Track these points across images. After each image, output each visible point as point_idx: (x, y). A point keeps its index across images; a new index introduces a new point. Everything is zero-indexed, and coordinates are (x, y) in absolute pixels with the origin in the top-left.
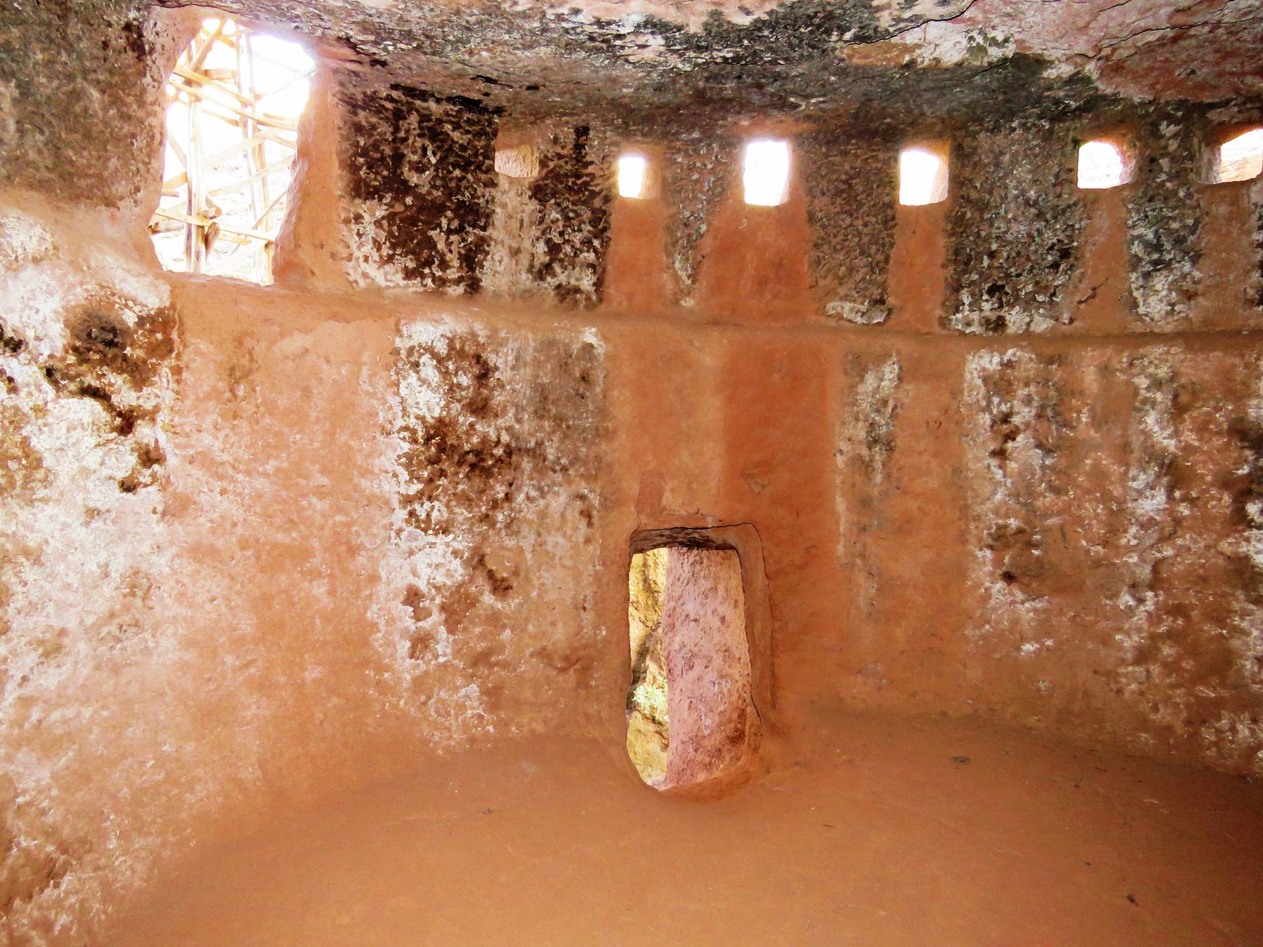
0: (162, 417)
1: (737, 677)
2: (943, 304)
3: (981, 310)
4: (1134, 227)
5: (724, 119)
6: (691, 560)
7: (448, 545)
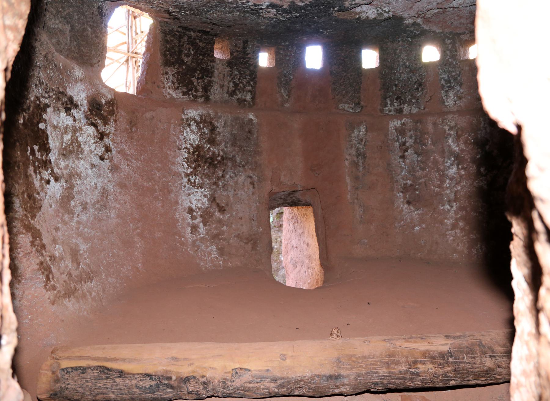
0: (111, 136)
1: (315, 267)
2: (381, 104)
3: (394, 106)
4: (441, 75)
5: (297, 37)
6: (293, 222)
7: (202, 192)
